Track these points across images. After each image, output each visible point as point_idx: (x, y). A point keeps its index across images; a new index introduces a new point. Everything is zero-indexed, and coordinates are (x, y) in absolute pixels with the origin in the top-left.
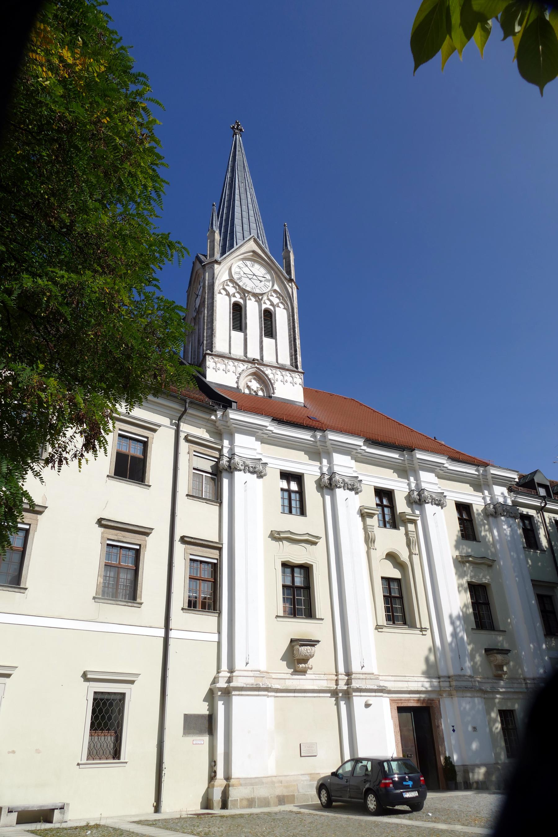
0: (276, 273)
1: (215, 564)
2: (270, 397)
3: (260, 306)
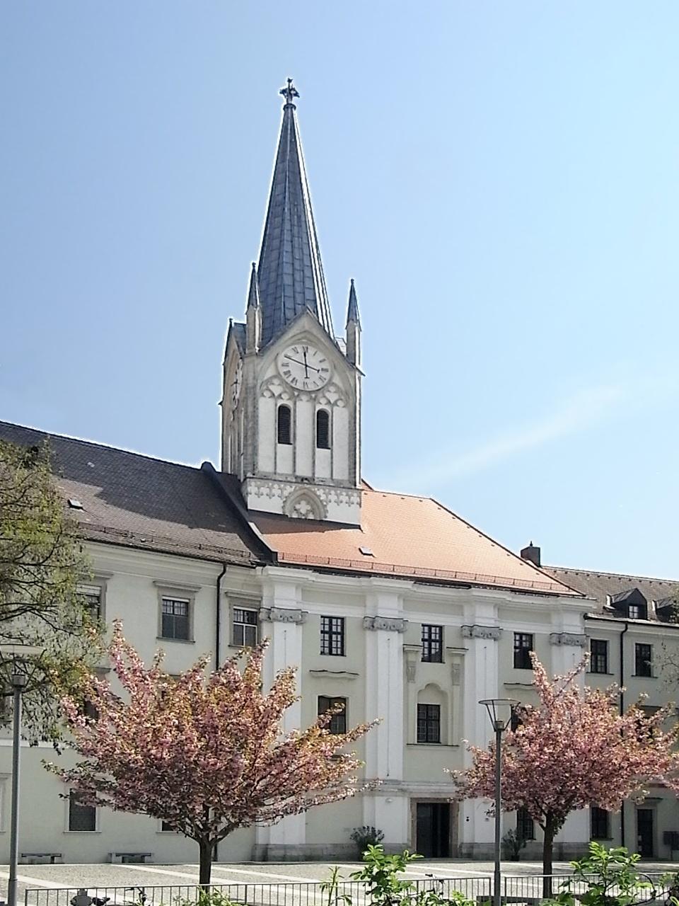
1: (187, 603)
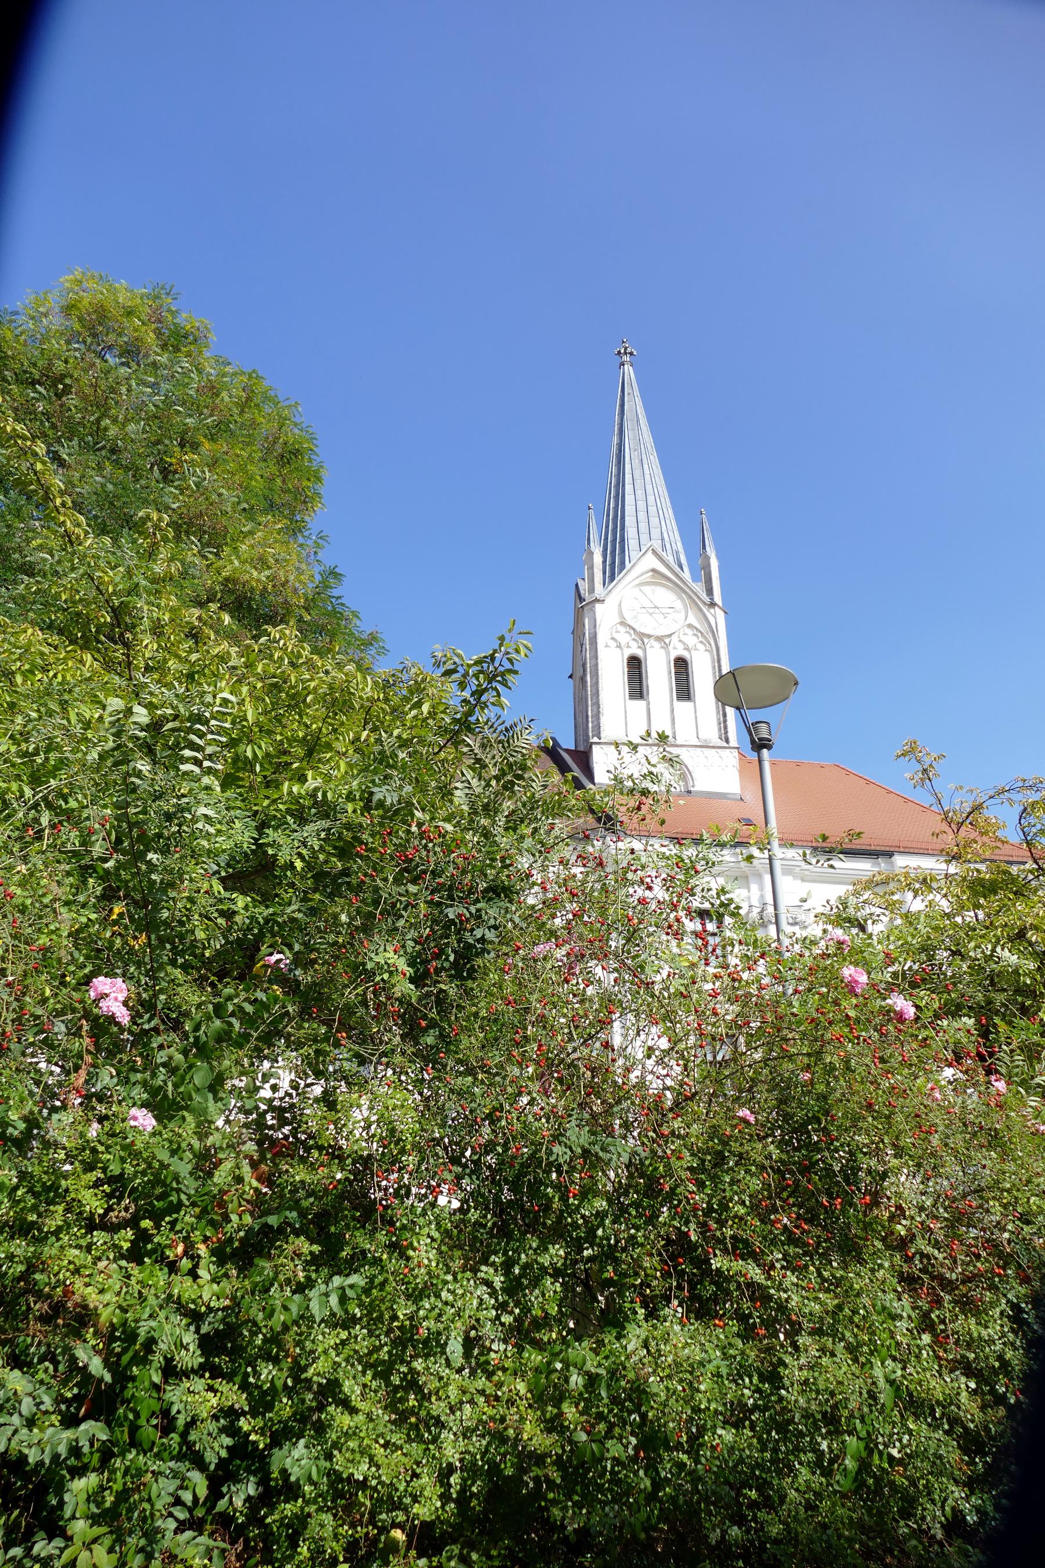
0: (690, 597)
2: (689, 792)
3: (668, 653)
